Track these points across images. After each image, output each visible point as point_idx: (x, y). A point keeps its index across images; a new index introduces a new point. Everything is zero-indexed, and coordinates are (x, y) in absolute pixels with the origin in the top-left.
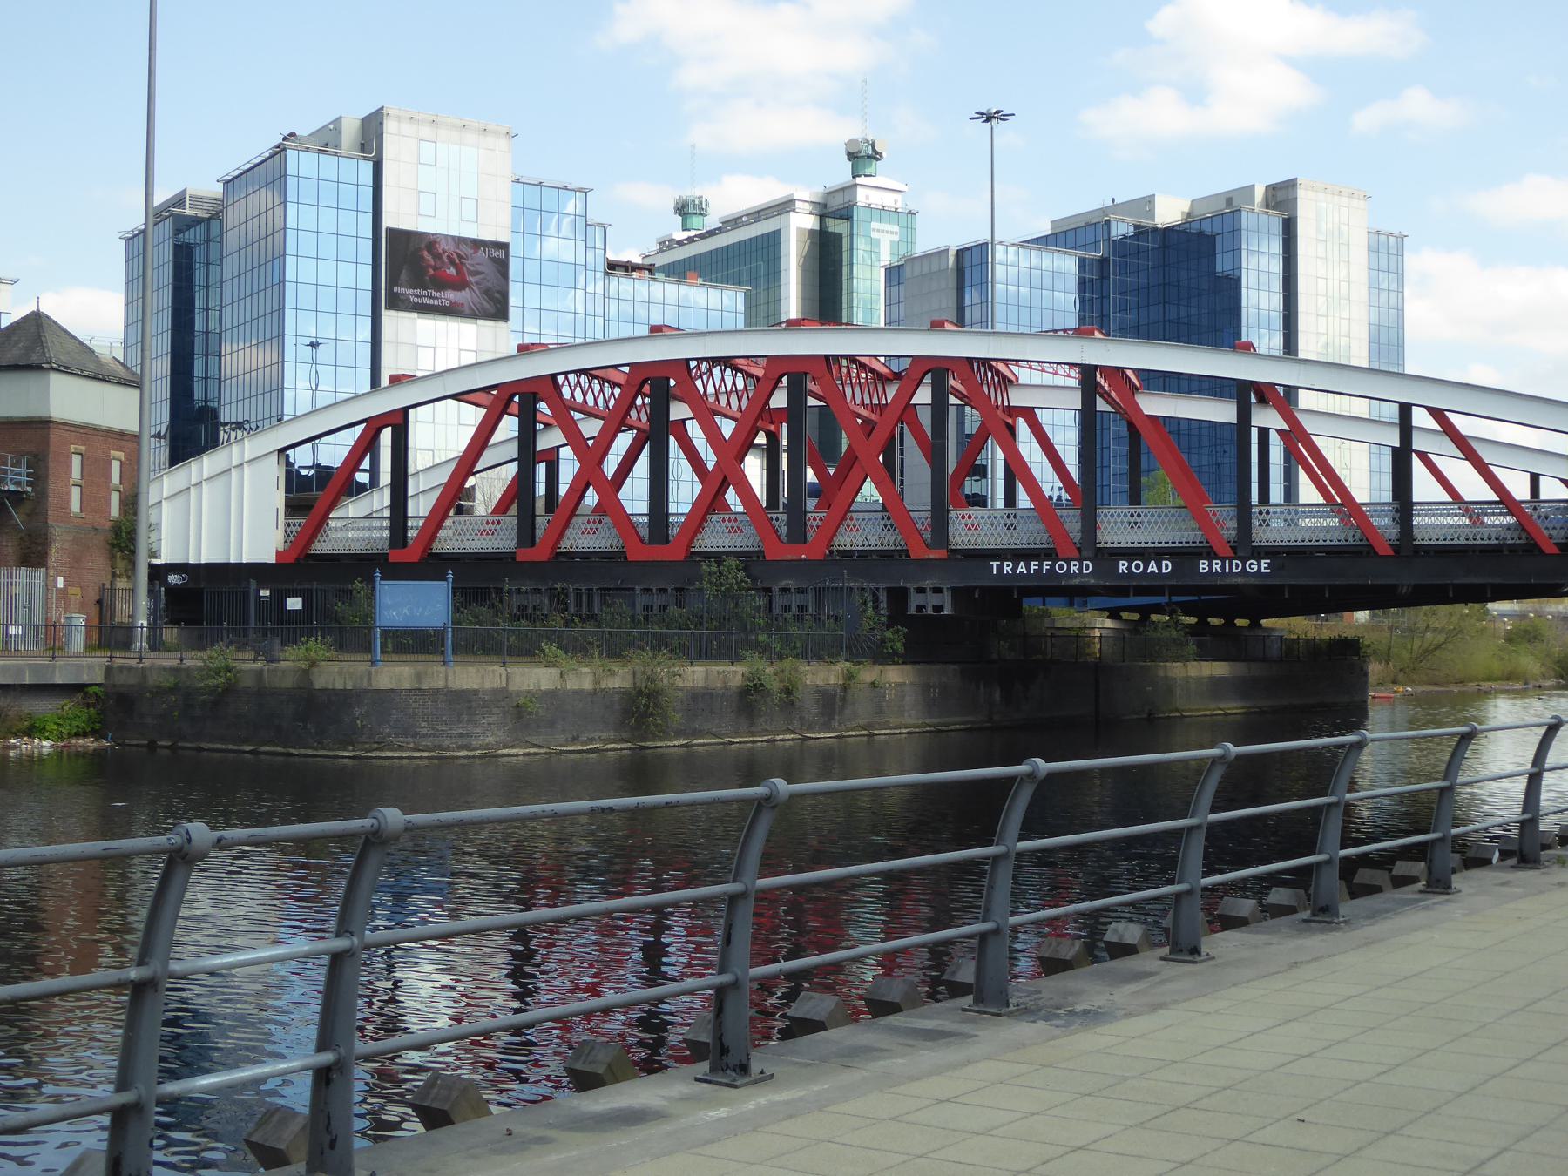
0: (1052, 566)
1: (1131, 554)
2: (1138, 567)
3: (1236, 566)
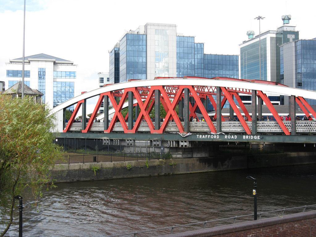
1: (227, 133)
3: (252, 137)
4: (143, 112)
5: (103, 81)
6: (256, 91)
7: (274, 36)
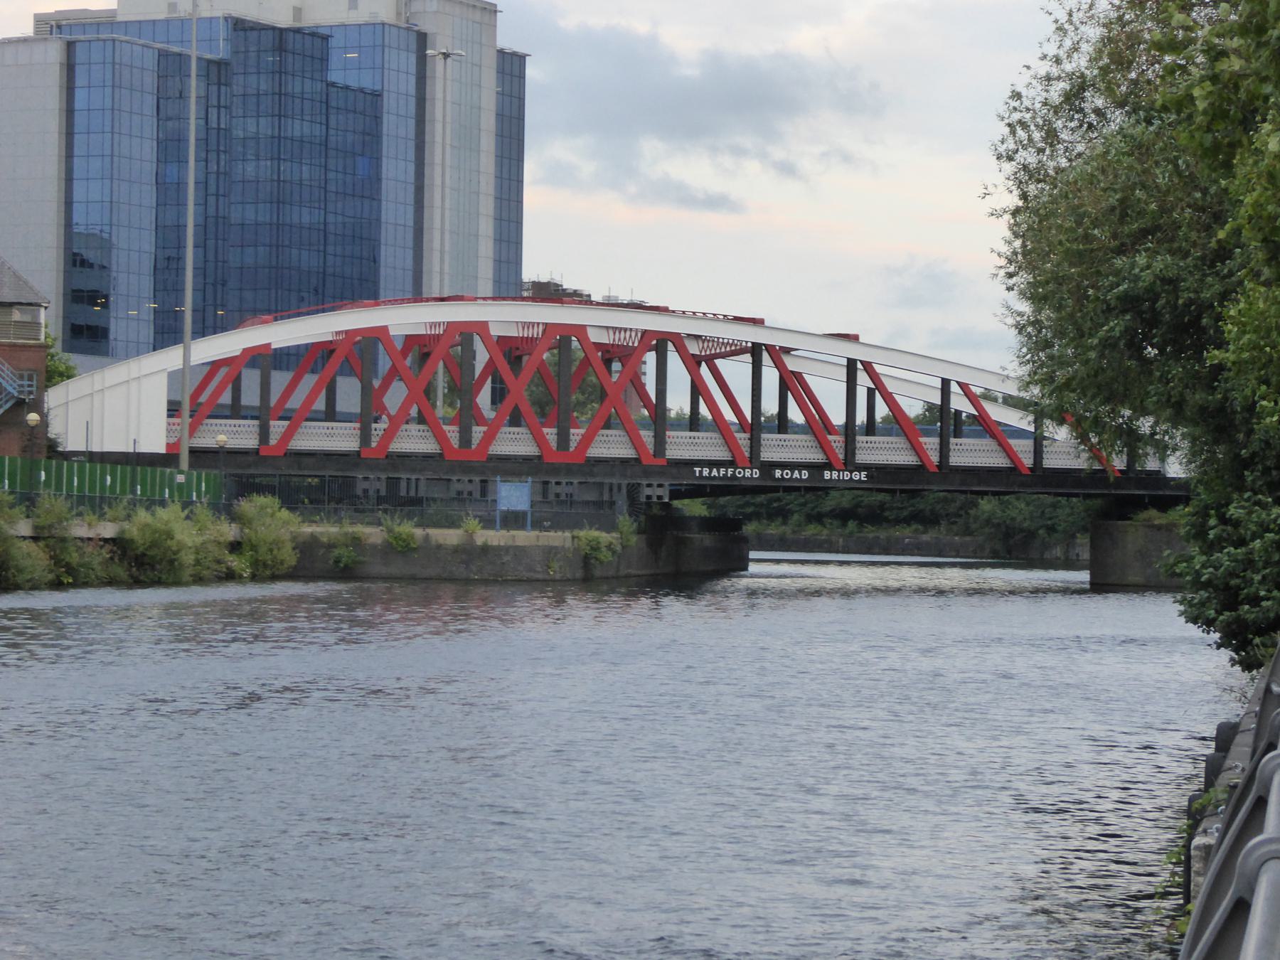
0: (734, 472)
3: (847, 476)
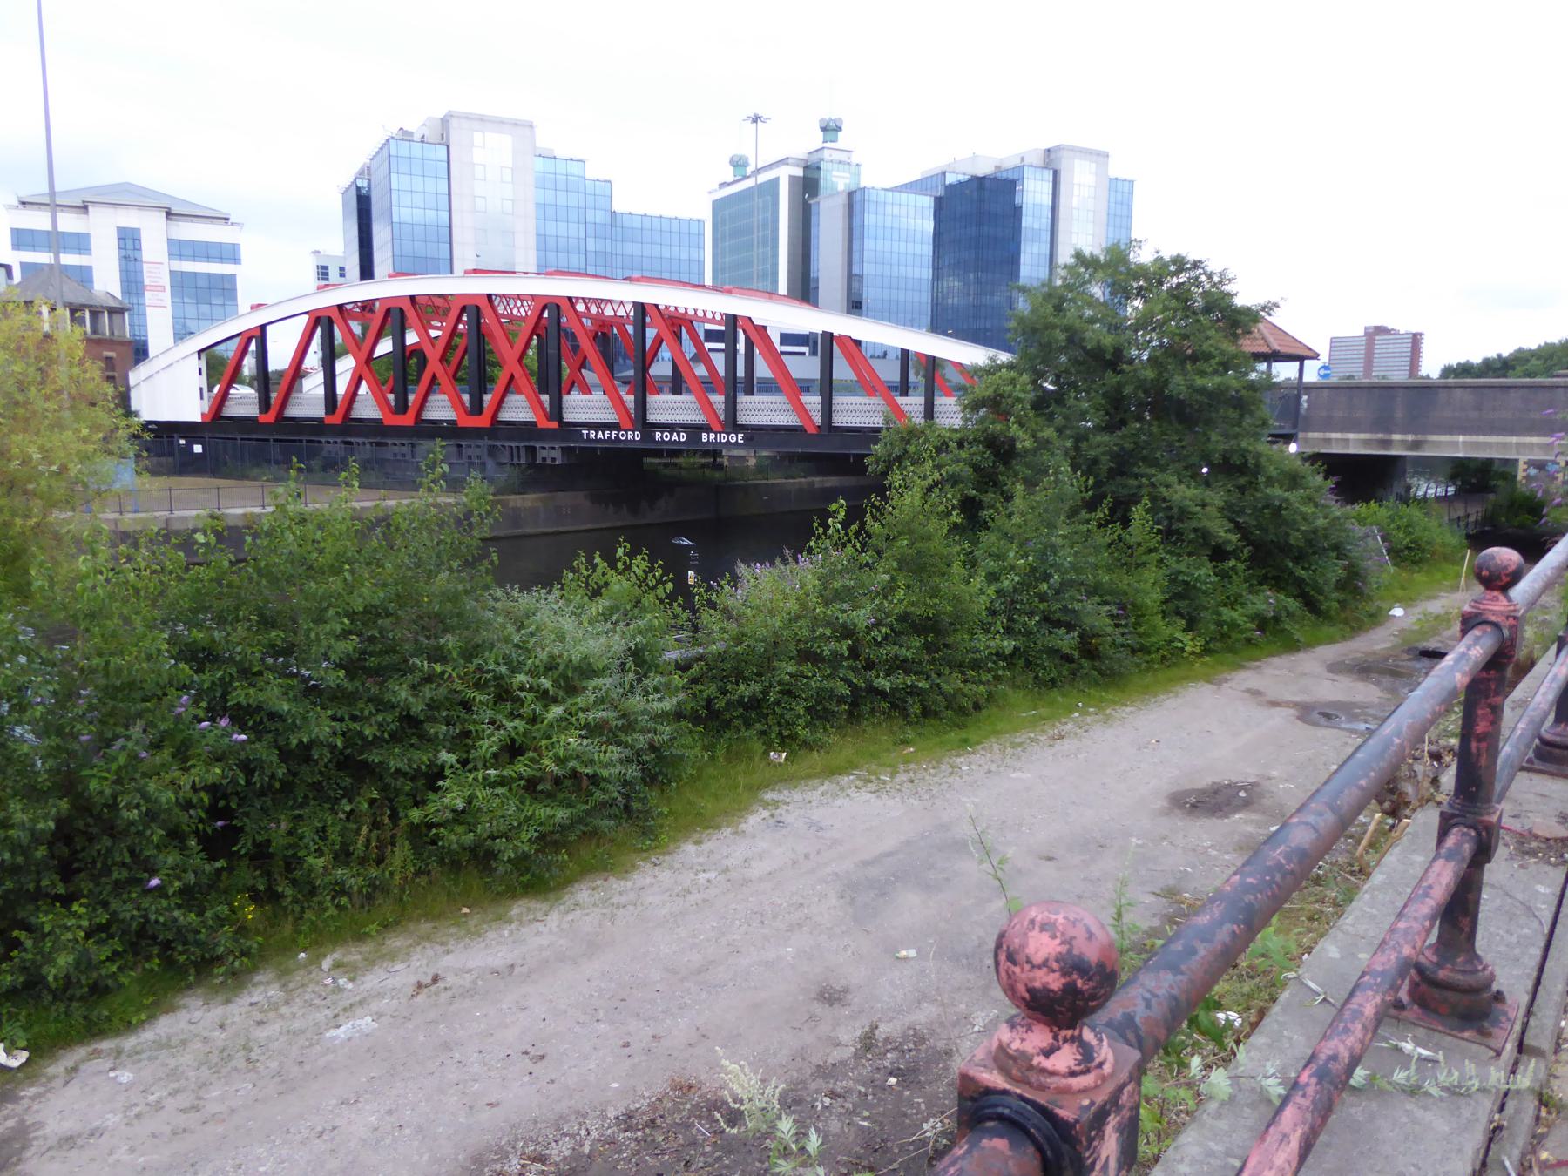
1: (663, 427)
2: (666, 436)
3: (724, 438)
4: (434, 366)
5: (327, 274)
6: (735, 317)
7: (799, 172)
